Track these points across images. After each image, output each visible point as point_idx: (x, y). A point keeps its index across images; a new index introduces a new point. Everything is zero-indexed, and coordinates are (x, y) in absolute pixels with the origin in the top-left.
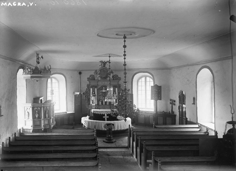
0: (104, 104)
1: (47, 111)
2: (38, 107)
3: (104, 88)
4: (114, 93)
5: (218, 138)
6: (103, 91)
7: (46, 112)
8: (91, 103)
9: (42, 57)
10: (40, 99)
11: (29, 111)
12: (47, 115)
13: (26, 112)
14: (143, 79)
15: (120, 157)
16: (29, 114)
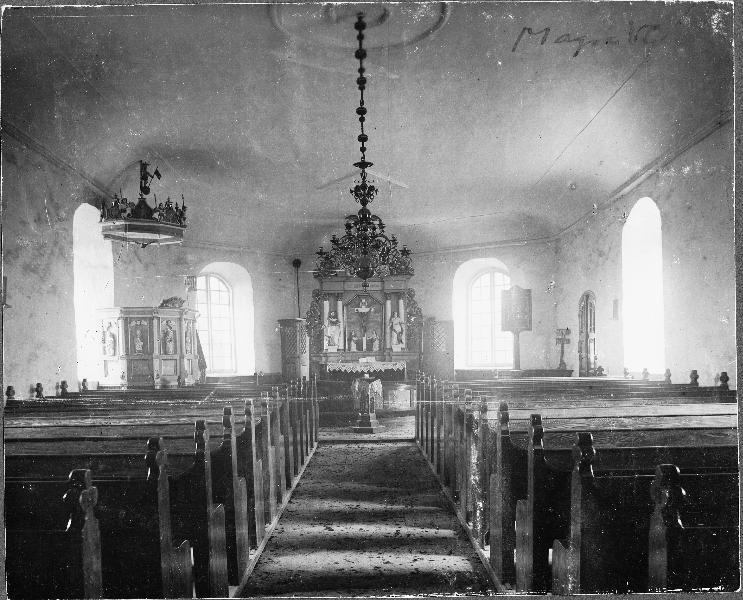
0: (365, 347)
1: (171, 334)
2: (140, 319)
3: (364, 301)
4: (393, 316)
5: (700, 385)
6: (360, 310)
7: (166, 334)
8: (326, 343)
9: (157, 173)
10: (404, 346)
11: (114, 330)
12: (170, 346)
13: (108, 334)
14: (486, 278)
15: (306, 358)
16: (115, 341)
